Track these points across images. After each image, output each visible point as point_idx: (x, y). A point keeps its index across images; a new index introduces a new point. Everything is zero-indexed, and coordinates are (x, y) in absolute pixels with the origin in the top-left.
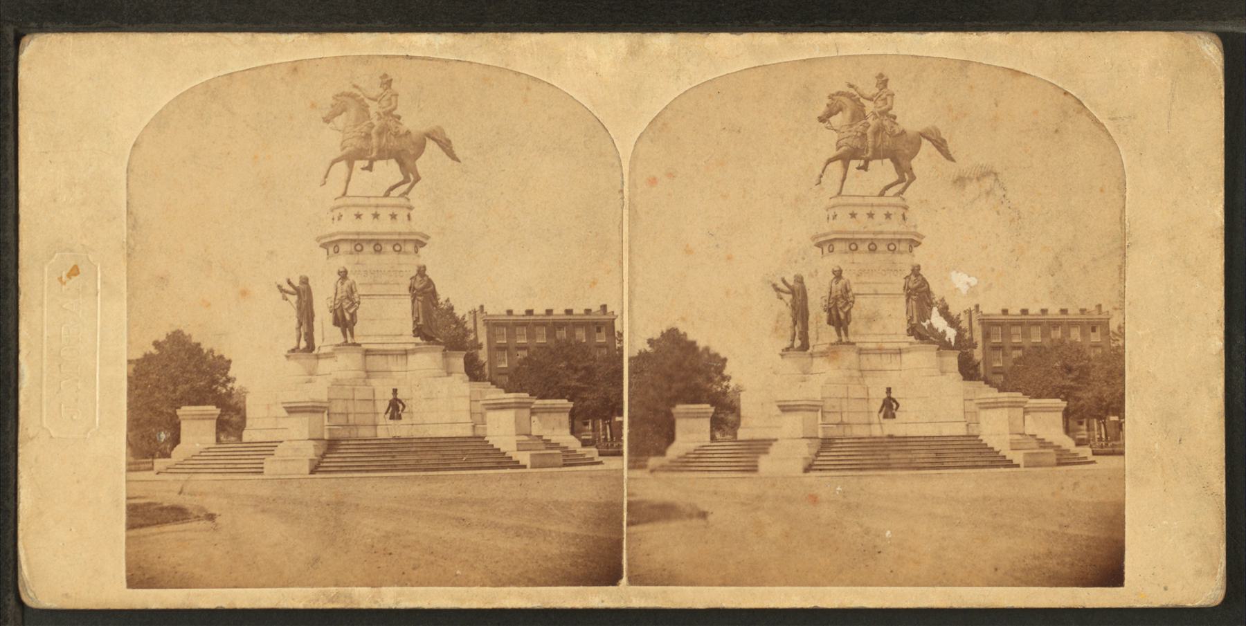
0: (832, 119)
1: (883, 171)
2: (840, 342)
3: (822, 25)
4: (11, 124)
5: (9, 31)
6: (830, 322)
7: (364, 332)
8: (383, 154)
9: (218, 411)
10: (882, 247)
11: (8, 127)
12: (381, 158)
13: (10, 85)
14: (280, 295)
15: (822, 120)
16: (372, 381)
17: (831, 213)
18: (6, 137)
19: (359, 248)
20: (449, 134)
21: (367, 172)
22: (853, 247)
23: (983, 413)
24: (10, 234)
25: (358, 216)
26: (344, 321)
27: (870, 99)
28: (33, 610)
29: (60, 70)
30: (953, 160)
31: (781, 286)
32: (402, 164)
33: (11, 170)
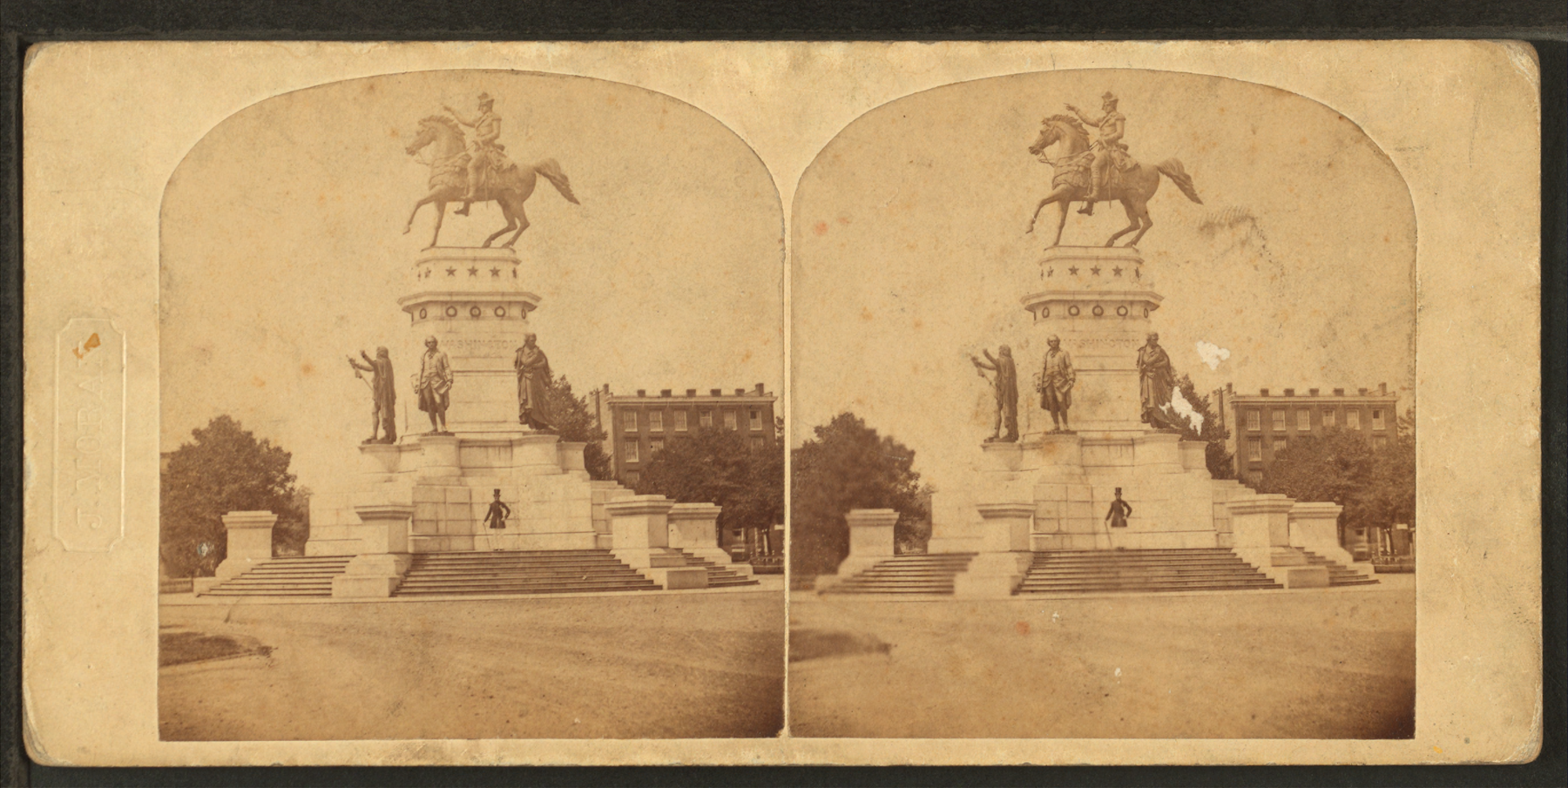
0: (1047, 150)
1: (1111, 215)
2: (1057, 431)
3: (1034, 32)
4: (14, 155)
6: (1045, 406)
7: (458, 417)
10: (1110, 311)
11: (10, 159)
12: (479, 199)
13: (13, 107)
14: (352, 372)
15: (1034, 151)
17: (1046, 268)
18: (8, 173)
19: (451, 312)
20: (565, 169)
21: (461, 216)
22: (1074, 311)
23: (1237, 520)
24: (13, 294)
25: (451, 272)
26: (433, 405)
28: (41, 767)
29: (75, 88)
30: (1199, 202)
31: (983, 359)
32: (505, 206)
33: (14, 214)
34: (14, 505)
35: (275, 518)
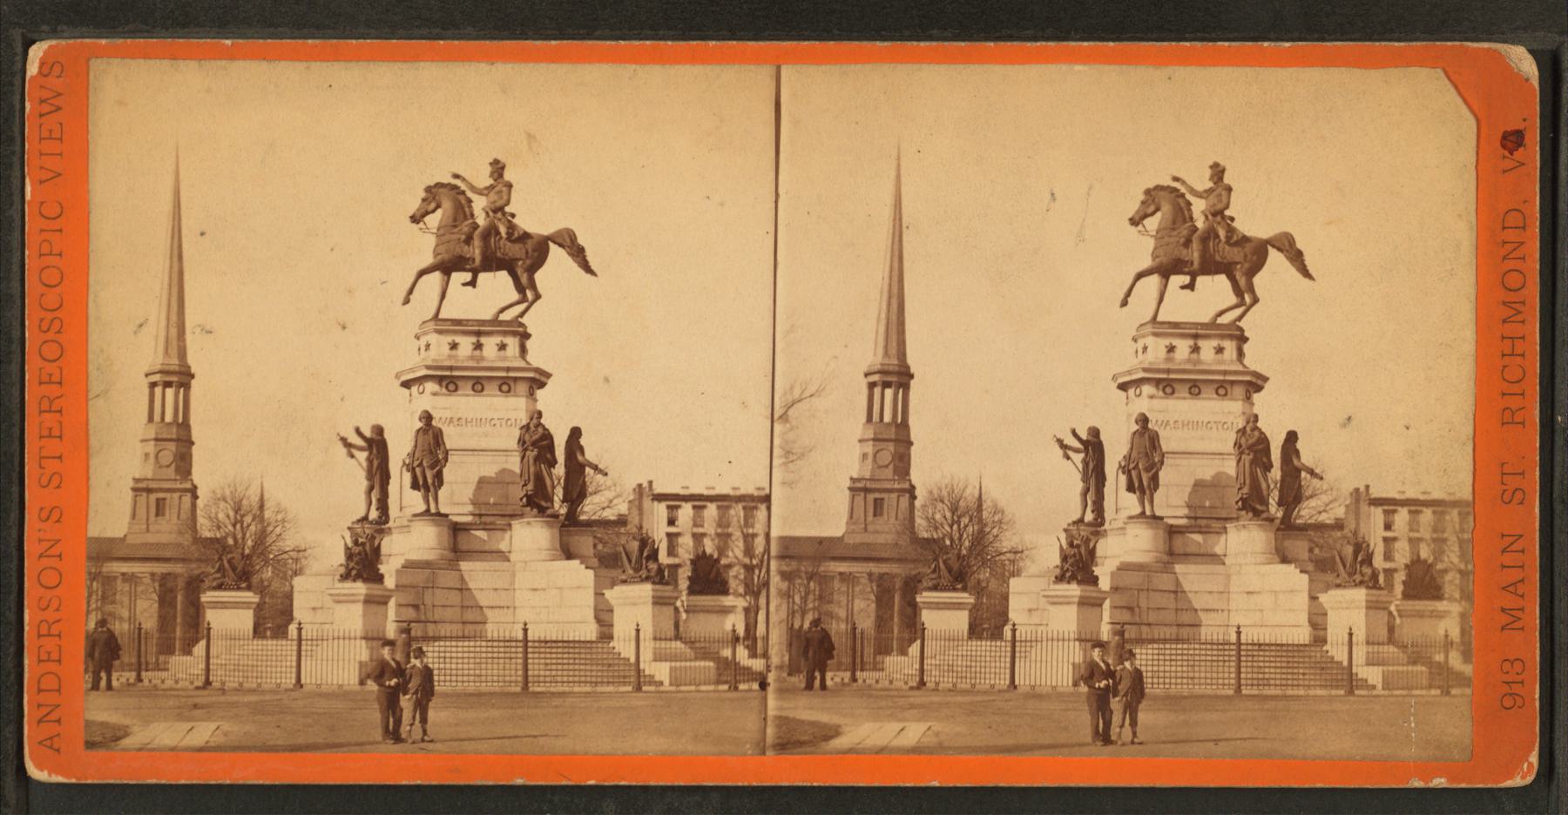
0: (427, 219)
6: (1130, 488)
8: (492, 262)
12: (485, 270)
16: (1178, 568)
17: (1140, 345)
21: (1188, 291)
23: (338, 607)
27: (480, 192)
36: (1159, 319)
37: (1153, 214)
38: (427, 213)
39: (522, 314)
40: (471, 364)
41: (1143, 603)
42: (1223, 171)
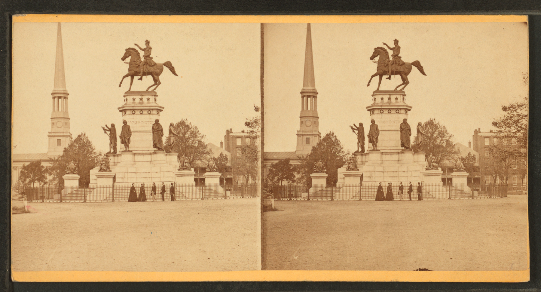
2: (374, 150)
5: (7, 14)
9: (79, 177)
12: (145, 75)
14: (104, 131)
17: (374, 97)
18: (5, 61)
21: (388, 80)
24: (7, 103)
30: (177, 75)
31: (106, 128)
34: (8, 176)
35: (79, 177)
36: (132, 90)
37: (128, 57)
38: (375, 57)
39: (403, 88)
40: (139, 105)
41: (373, 175)
42: (398, 42)
